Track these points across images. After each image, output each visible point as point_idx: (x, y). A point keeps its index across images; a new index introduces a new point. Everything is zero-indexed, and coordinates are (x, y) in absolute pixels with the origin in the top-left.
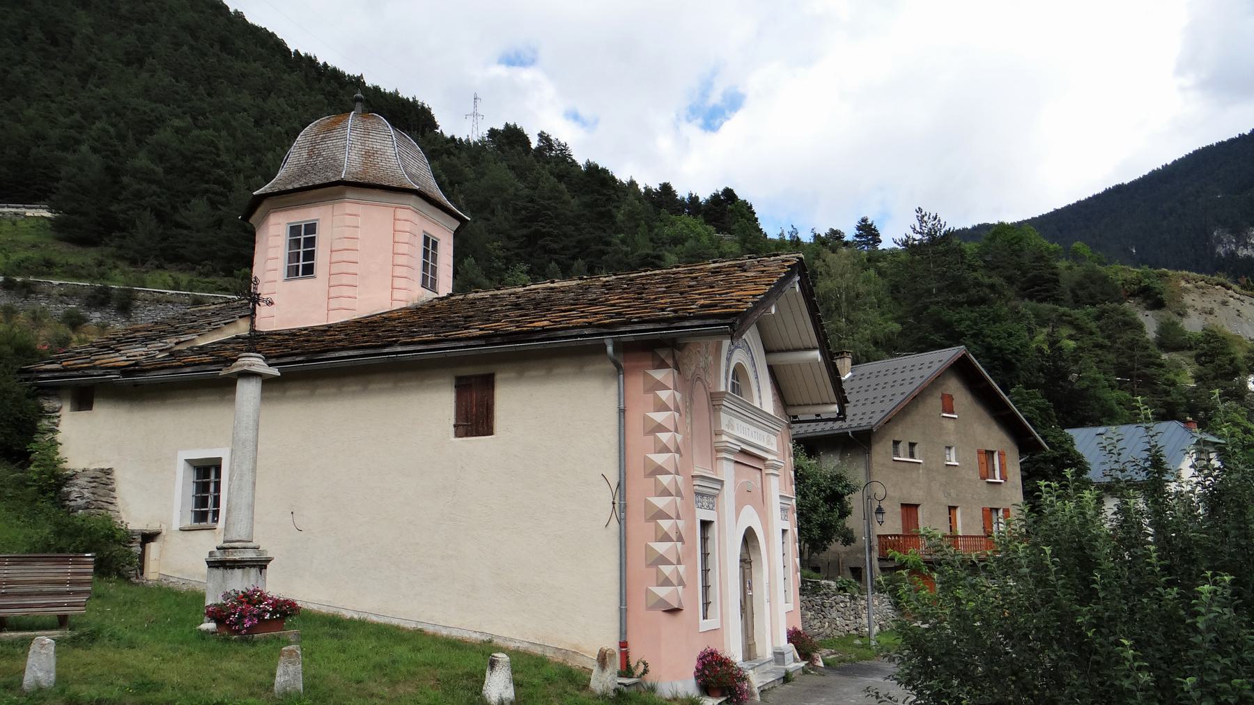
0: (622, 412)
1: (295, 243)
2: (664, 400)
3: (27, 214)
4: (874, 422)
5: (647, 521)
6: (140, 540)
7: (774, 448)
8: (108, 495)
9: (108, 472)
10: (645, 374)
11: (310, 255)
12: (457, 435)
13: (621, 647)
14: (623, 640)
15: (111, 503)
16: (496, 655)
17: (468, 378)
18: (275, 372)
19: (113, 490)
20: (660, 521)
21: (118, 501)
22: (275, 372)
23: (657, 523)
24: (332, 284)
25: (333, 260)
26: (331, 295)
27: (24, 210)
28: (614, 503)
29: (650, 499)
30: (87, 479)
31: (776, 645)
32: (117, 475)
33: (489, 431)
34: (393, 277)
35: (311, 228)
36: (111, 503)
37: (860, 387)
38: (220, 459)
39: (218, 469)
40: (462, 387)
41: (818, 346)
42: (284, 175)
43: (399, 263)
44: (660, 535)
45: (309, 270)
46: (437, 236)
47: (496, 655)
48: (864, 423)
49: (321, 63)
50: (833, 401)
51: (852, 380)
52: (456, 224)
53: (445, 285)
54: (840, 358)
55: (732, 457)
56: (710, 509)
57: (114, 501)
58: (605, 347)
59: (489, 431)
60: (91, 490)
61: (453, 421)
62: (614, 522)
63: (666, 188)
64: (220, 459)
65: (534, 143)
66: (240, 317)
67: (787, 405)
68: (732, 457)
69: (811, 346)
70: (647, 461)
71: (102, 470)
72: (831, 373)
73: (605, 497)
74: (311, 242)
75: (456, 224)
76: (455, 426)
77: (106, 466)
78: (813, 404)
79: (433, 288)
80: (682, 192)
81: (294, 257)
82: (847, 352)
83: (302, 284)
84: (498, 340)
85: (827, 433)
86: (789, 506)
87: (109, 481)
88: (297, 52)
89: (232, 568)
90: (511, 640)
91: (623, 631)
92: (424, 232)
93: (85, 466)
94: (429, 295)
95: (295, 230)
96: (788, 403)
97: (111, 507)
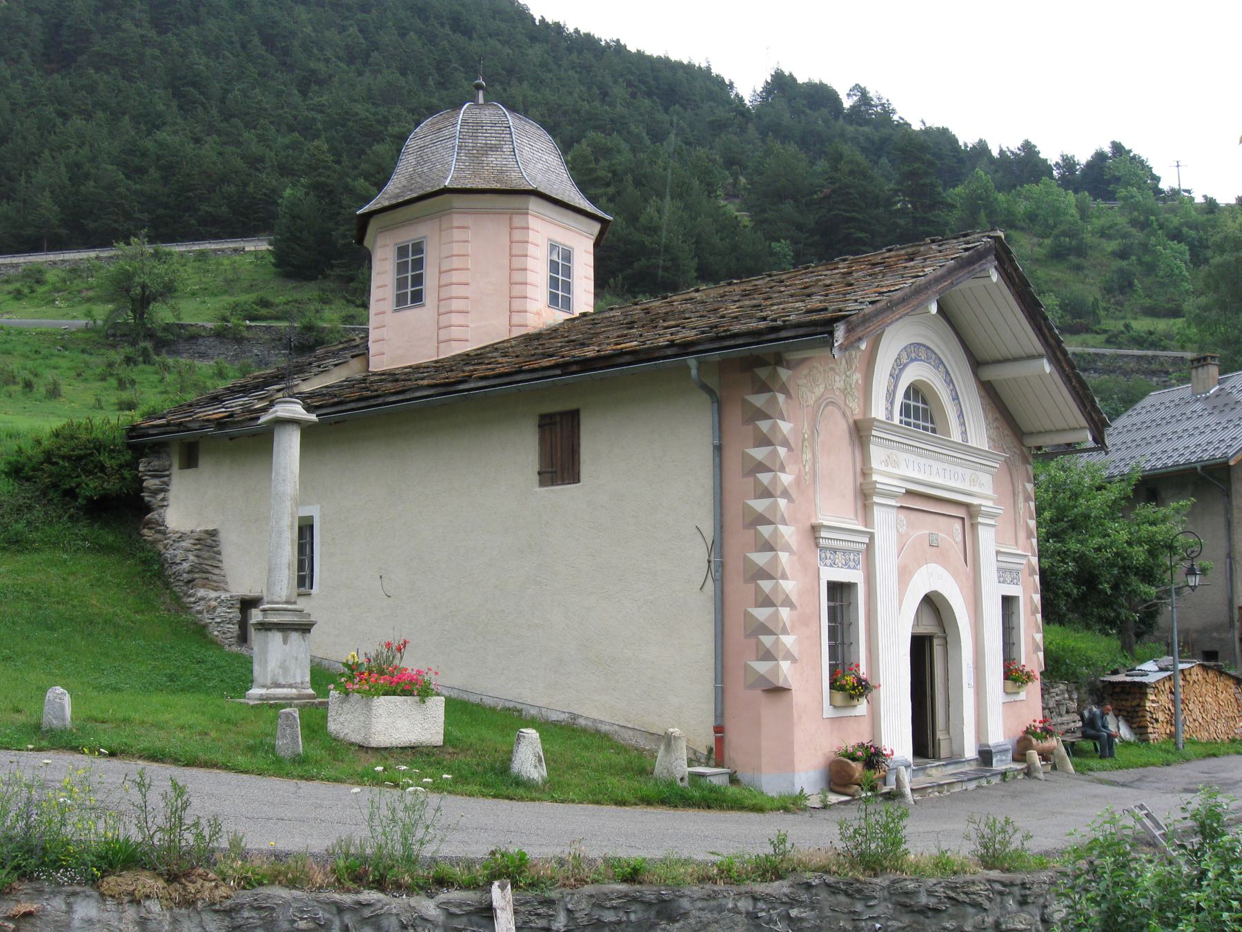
0: (719, 449)
1: (401, 268)
2: (765, 431)
3: (247, 249)
4: (1231, 452)
5: (746, 581)
6: (239, 606)
7: (988, 490)
8: (214, 558)
9: (213, 534)
10: (745, 402)
11: (418, 280)
12: (542, 483)
13: (716, 732)
14: (719, 723)
15: (217, 567)
16: (523, 730)
17: (551, 416)
18: (313, 417)
19: (219, 553)
20: (760, 582)
21: (225, 565)
22: (313, 417)
23: (757, 585)
24: (442, 311)
25: (442, 283)
26: (441, 325)
27: (242, 244)
28: (709, 562)
29: (749, 555)
30: (193, 541)
31: (983, 742)
32: (223, 536)
33: (574, 477)
34: (511, 298)
35: (418, 248)
36: (217, 567)
37: (1226, 405)
38: (312, 518)
39: (312, 527)
40: (547, 424)
41: (1044, 352)
42: (395, 188)
43: (518, 281)
44: (760, 599)
45: (418, 297)
46: (568, 243)
47: (523, 730)
48: (1218, 454)
49: (571, 30)
50: (1073, 424)
51: (1217, 396)
52: (596, 227)
53: (583, 298)
54: (1203, 366)
55: (893, 502)
56: (849, 567)
57: (220, 565)
58: (688, 368)
59: (574, 477)
60: (195, 552)
61: (536, 468)
62: (710, 582)
63: (1028, 147)
64: (312, 518)
65: (847, 103)
66: (353, 357)
67: (1023, 434)
68: (893, 502)
69: (1035, 353)
70: (748, 510)
71: (207, 532)
72: (1074, 388)
73: (699, 554)
74: (419, 264)
75: (596, 227)
76: (539, 473)
77: (210, 528)
78: (1058, 431)
79: (567, 305)
80: (1050, 153)
81: (401, 284)
82: (1212, 357)
83: (412, 315)
84: (574, 368)
85: (1169, 469)
86: (1022, 566)
87: (214, 544)
88: (543, 21)
89: (270, 630)
90: (601, 722)
91: (720, 713)
92: (549, 239)
93: (193, 528)
94: (558, 317)
95: (402, 251)
96: (1025, 429)
97: (216, 571)
